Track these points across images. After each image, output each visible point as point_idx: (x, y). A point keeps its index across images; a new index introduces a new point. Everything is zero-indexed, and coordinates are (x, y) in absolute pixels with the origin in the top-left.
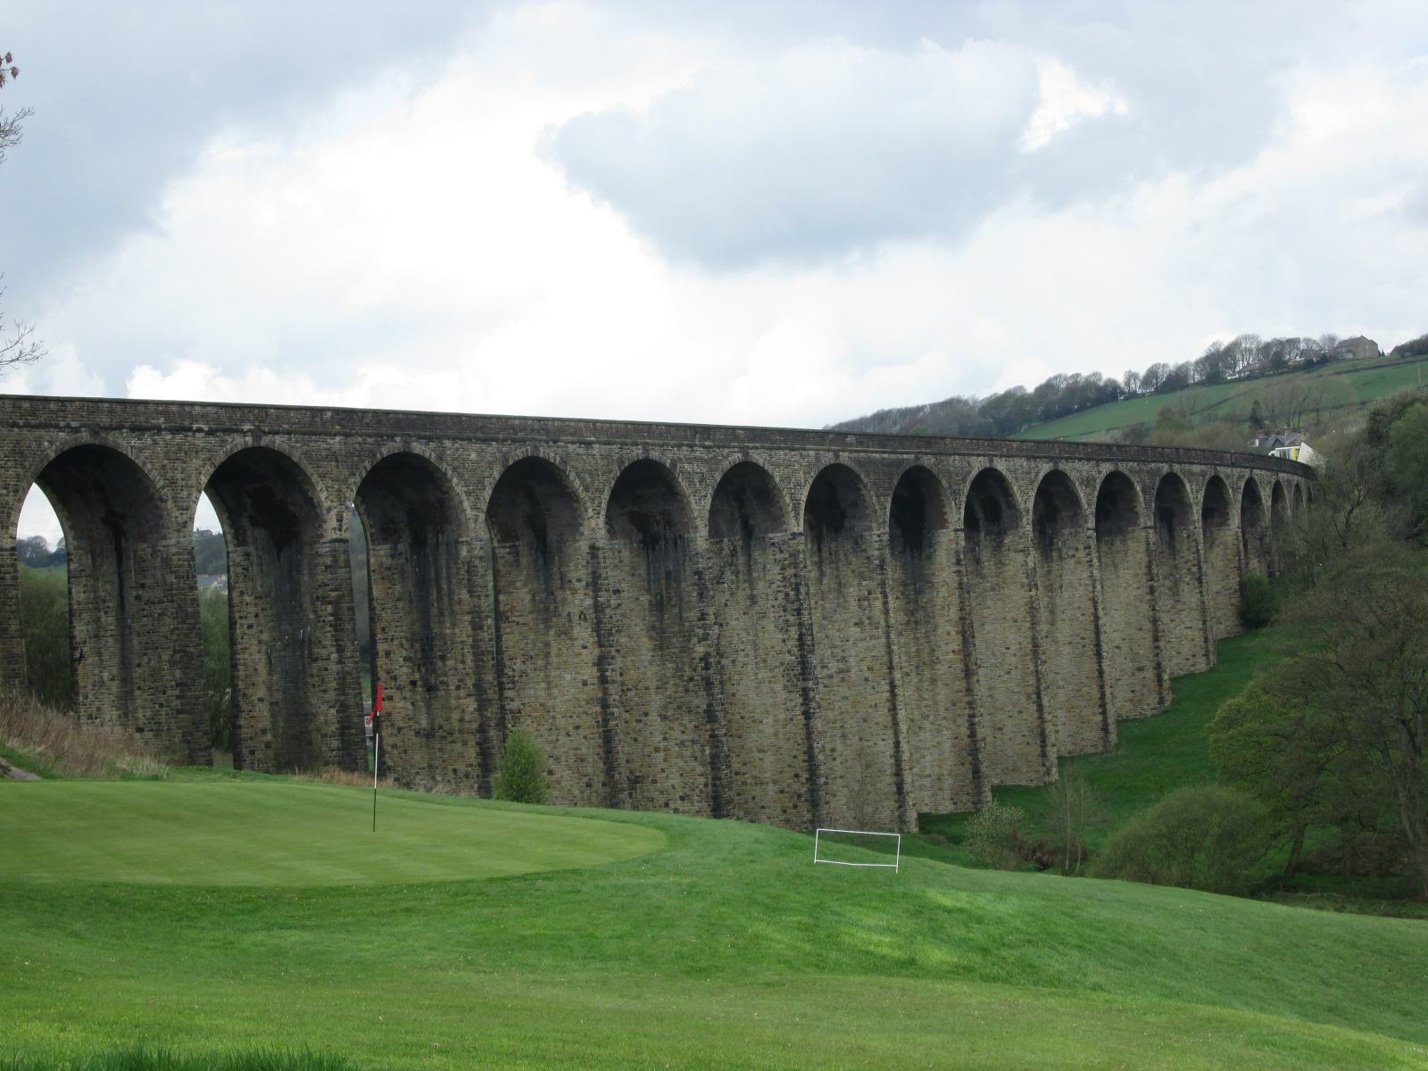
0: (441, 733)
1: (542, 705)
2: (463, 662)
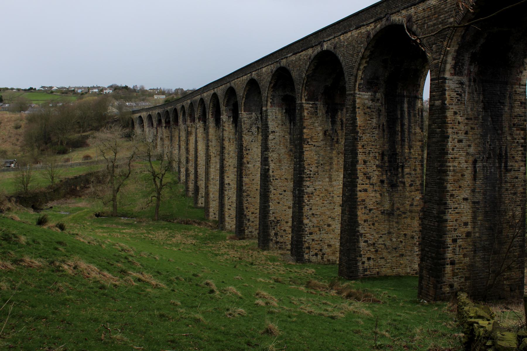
0: (398, 212)
1: (326, 190)
2: (415, 170)
